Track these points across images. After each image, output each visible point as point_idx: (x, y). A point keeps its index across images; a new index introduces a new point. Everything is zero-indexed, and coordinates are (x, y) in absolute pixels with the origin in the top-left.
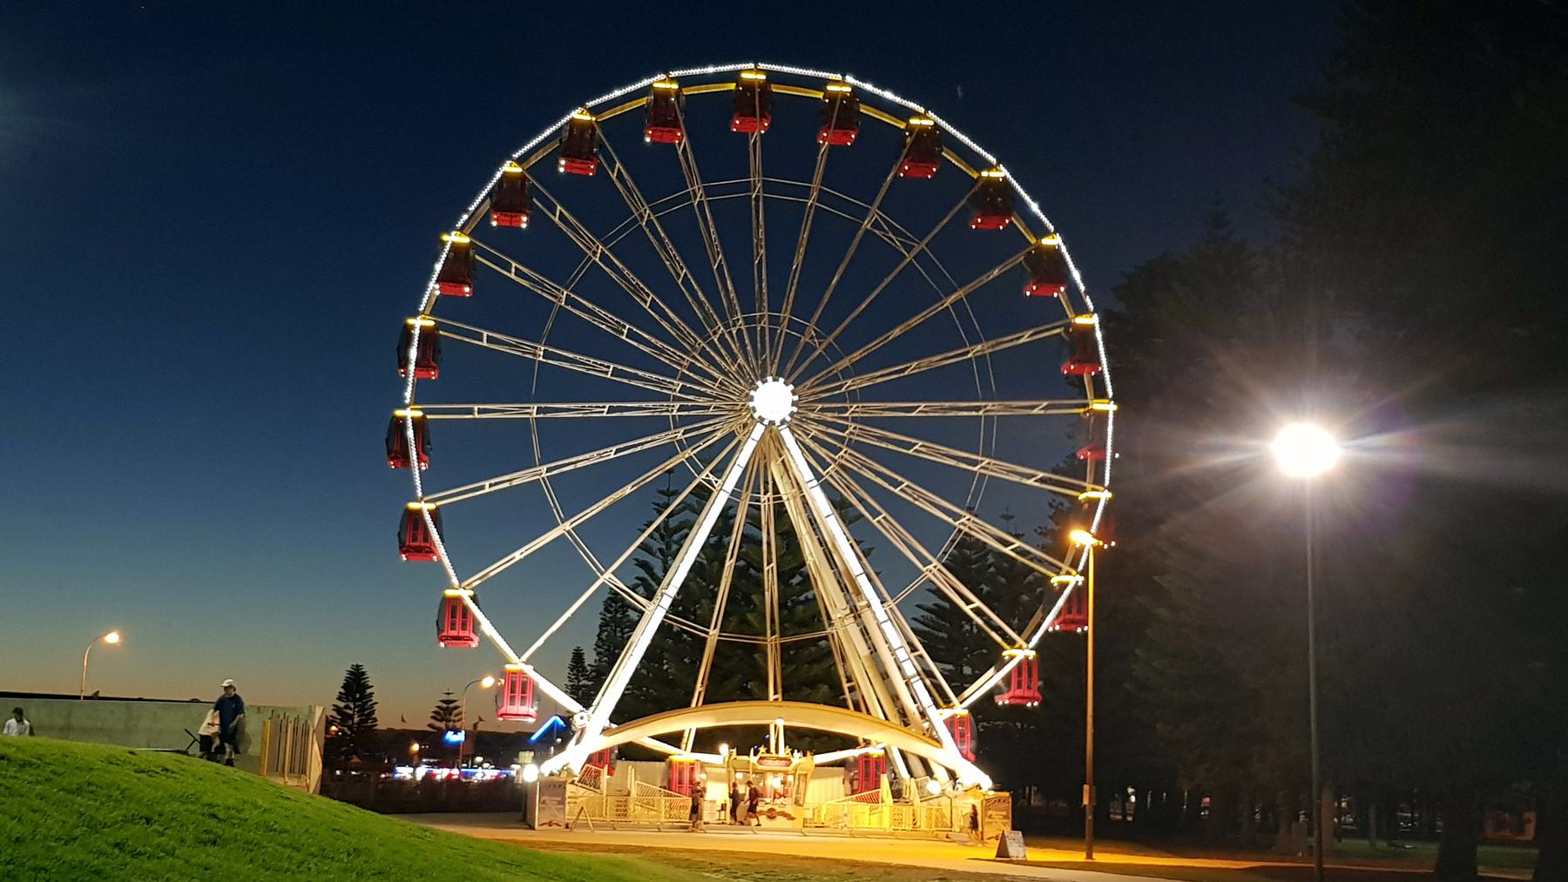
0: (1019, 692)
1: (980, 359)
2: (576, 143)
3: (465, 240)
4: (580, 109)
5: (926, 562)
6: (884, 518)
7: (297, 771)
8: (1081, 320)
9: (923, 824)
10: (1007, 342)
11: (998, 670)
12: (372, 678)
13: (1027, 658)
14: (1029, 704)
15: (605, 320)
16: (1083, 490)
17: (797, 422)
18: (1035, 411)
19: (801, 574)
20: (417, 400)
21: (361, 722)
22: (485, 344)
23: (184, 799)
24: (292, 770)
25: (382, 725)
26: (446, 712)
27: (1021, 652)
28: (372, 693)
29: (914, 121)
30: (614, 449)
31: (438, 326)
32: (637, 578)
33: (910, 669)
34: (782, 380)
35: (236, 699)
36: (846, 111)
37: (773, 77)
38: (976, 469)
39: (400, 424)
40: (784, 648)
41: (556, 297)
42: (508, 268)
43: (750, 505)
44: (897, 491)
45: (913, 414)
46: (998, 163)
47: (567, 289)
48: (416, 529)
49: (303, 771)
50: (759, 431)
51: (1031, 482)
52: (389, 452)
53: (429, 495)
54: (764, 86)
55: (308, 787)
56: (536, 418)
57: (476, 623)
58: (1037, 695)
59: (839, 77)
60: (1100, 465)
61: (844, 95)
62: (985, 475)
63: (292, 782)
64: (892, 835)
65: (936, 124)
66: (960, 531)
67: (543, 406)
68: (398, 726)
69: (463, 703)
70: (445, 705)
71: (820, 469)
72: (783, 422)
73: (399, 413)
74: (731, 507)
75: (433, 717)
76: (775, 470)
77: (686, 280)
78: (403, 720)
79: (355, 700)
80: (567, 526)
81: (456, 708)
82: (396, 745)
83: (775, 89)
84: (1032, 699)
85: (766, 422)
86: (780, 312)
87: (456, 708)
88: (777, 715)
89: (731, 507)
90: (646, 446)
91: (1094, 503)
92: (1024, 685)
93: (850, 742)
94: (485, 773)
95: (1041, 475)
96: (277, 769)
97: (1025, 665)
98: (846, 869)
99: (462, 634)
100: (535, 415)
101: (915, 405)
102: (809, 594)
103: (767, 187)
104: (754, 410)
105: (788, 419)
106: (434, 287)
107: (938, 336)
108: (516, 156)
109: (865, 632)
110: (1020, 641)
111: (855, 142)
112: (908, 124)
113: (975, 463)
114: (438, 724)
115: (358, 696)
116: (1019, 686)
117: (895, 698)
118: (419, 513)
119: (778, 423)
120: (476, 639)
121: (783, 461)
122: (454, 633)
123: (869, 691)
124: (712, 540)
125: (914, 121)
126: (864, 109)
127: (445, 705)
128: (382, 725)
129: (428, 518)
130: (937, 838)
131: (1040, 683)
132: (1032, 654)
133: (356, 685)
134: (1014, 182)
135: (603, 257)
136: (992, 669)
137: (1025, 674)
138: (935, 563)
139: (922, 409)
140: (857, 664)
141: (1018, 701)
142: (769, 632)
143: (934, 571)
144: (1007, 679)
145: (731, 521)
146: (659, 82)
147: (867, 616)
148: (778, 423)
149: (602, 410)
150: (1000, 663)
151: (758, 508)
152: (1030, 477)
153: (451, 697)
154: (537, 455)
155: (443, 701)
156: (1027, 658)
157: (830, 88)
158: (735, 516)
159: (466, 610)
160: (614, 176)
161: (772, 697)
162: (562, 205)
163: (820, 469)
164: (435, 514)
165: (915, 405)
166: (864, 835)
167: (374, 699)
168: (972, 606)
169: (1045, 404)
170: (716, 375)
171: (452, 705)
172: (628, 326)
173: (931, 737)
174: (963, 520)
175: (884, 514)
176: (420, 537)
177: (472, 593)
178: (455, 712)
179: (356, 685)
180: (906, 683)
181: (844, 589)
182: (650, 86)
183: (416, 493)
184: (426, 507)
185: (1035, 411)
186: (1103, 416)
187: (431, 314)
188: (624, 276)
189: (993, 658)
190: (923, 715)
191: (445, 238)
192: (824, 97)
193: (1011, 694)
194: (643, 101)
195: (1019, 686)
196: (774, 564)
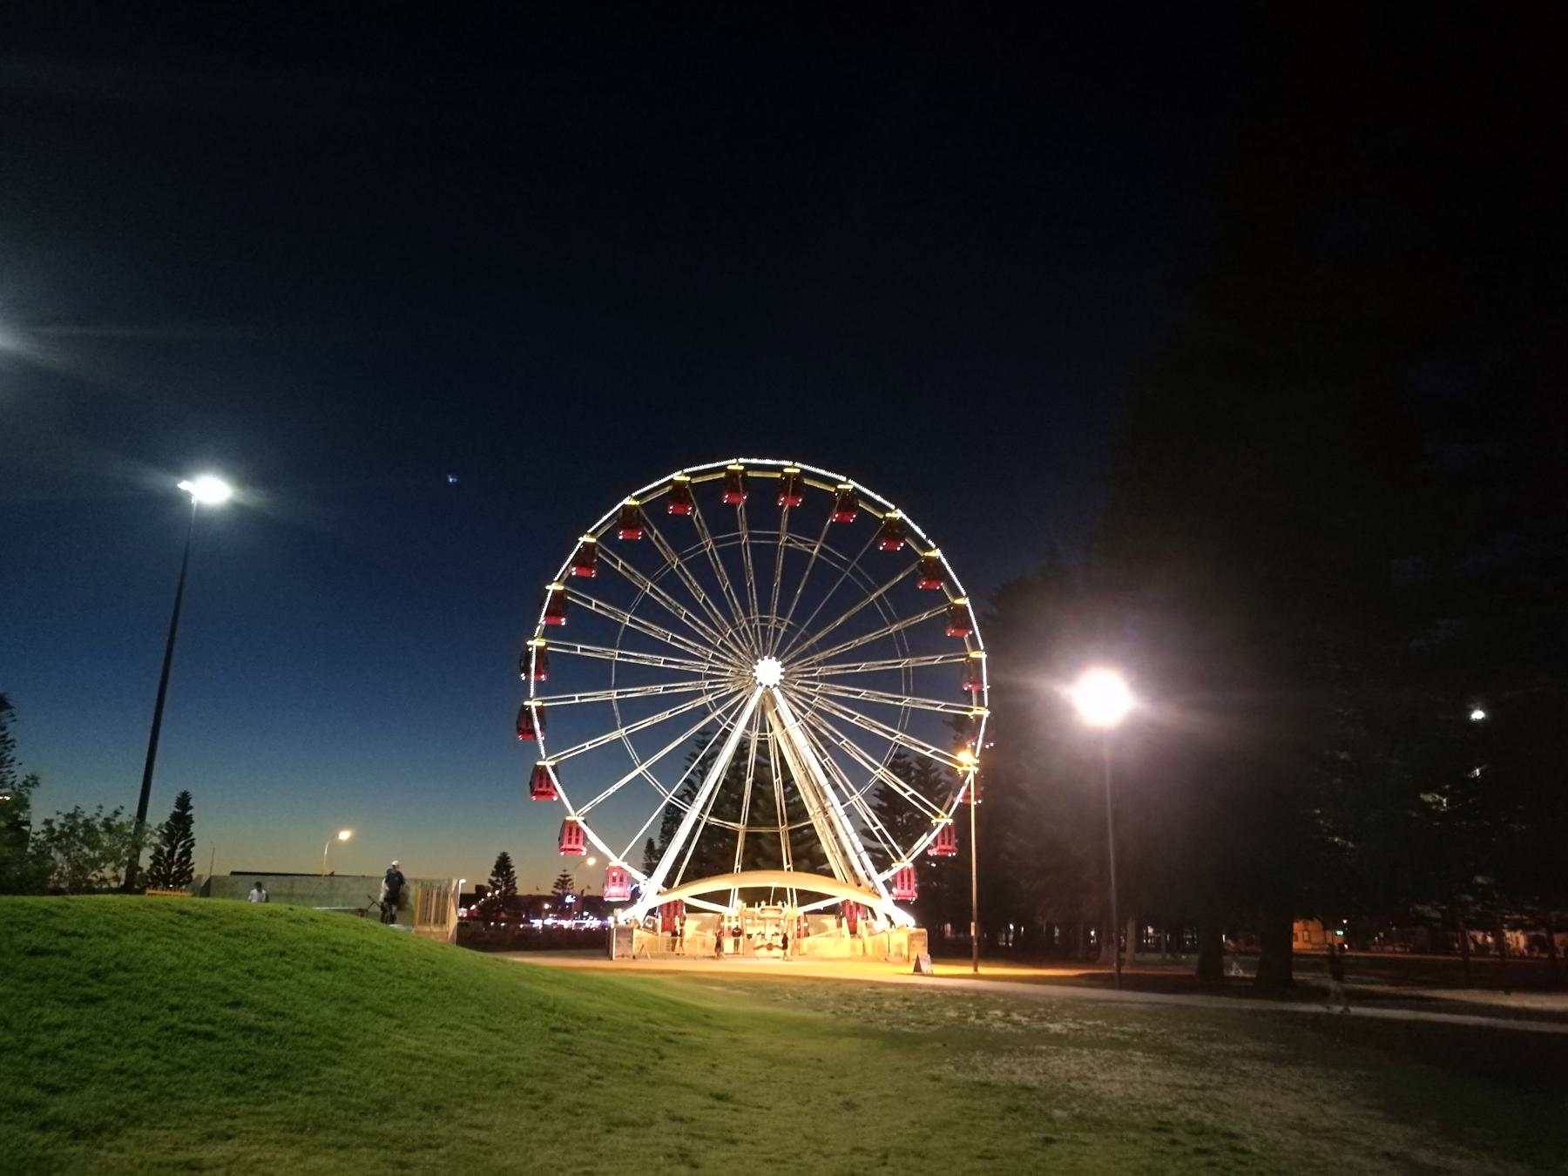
0: (943, 847)
1: (898, 632)
2: (628, 519)
3: (561, 588)
4: (628, 498)
5: (876, 768)
6: (846, 742)
7: (439, 921)
8: (959, 601)
9: (869, 950)
10: (914, 620)
11: (928, 835)
12: (514, 861)
13: (947, 824)
14: (950, 855)
15: (646, 659)
16: (972, 710)
17: (784, 686)
18: (936, 662)
19: (791, 786)
20: (537, 694)
21: (507, 890)
22: (579, 652)
23: (315, 939)
24: (436, 921)
25: (520, 892)
26: (564, 882)
27: (944, 820)
28: (513, 872)
29: (840, 486)
30: (668, 712)
31: (548, 645)
32: (685, 790)
33: (860, 848)
34: (774, 658)
35: (399, 875)
36: (795, 485)
37: (748, 467)
38: (902, 704)
39: (526, 713)
40: (791, 832)
41: (622, 619)
42: (590, 603)
43: (758, 741)
44: (853, 721)
45: (858, 670)
46: (896, 508)
47: (629, 613)
48: (541, 778)
49: (444, 922)
50: (759, 691)
51: (938, 709)
52: (519, 729)
53: (549, 756)
54: (743, 473)
55: (448, 933)
56: (617, 699)
57: (586, 838)
58: (955, 848)
59: (791, 463)
60: (980, 693)
61: (795, 474)
62: (908, 707)
63: (436, 929)
64: (849, 959)
65: (854, 487)
66: (896, 744)
67: (622, 652)
68: (535, 893)
69: (574, 877)
70: (562, 879)
71: (809, 701)
72: (775, 686)
73: (526, 703)
74: (745, 742)
75: (555, 887)
76: (770, 715)
77: (705, 601)
78: (538, 889)
79: (503, 876)
80: (643, 767)
81: (570, 880)
82: (533, 905)
83: (750, 474)
84: (952, 851)
85: (764, 686)
86: (721, 726)
87: (570, 880)
88: (789, 879)
89: (745, 742)
90: (684, 710)
91: (979, 718)
92: (946, 842)
93: (821, 897)
94: (593, 923)
95: (944, 704)
96: (425, 920)
97: (947, 828)
98: (810, 982)
99: (575, 847)
100: (616, 697)
101: (859, 664)
102: (796, 799)
103: (751, 536)
104: (756, 678)
105: (778, 684)
106: (542, 621)
107: (870, 619)
108: (590, 531)
109: (831, 825)
110: (942, 813)
111: (802, 503)
112: (837, 489)
113: (901, 700)
114: (557, 891)
115: (504, 873)
116: (943, 843)
117: (851, 868)
118: (544, 767)
119: (771, 687)
120: (585, 849)
121: (777, 712)
122: (570, 846)
123: (835, 862)
124: (734, 763)
125: (840, 486)
126: (806, 482)
127: (562, 879)
128: (520, 892)
129: (550, 771)
130: (878, 960)
131: (957, 841)
132: (950, 821)
133: (503, 866)
134: (909, 521)
135: (652, 589)
136: (925, 835)
137: (946, 833)
138: (882, 768)
139: (863, 667)
140: (827, 846)
141: (943, 853)
142: (780, 824)
143: (882, 773)
144: (935, 840)
145: (746, 751)
146: (677, 476)
147: (831, 812)
148: (771, 687)
149: (660, 689)
150: (930, 830)
151: (766, 742)
152: (937, 705)
153: (567, 873)
154: (619, 723)
155: (562, 876)
156: (947, 824)
157: (786, 470)
158: (749, 747)
159: (579, 830)
160: (653, 539)
161: (786, 867)
162: (623, 560)
163: (809, 701)
164: (554, 768)
165: (859, 664)
166: (824, 959)
167: (515, 875)
168: (909, 793)
169: (941, 657)
170: (727, 668)
171: (567, 878)
172: (671, 634)
173: (875, 893)
174: (897, 737)
175: (846, 740)
176: (545, 784)
177: (583, 818)
178: (570, 883)
179: (503, 866)
180: (859, 857)
181: (817, 797)
182: (672, 479)
183: (529, 695)
184: (548, 764)
185: (936, 662)
186: (978, 662)
187: (543, 637)
188: (666, 600)
189: (924, 826)
190: (869, 878)
191: (548, 587)
192: (782, 476)
193: (938, 848)
194: (668, 488)
195: (943, 843)
196: (780, 778)
